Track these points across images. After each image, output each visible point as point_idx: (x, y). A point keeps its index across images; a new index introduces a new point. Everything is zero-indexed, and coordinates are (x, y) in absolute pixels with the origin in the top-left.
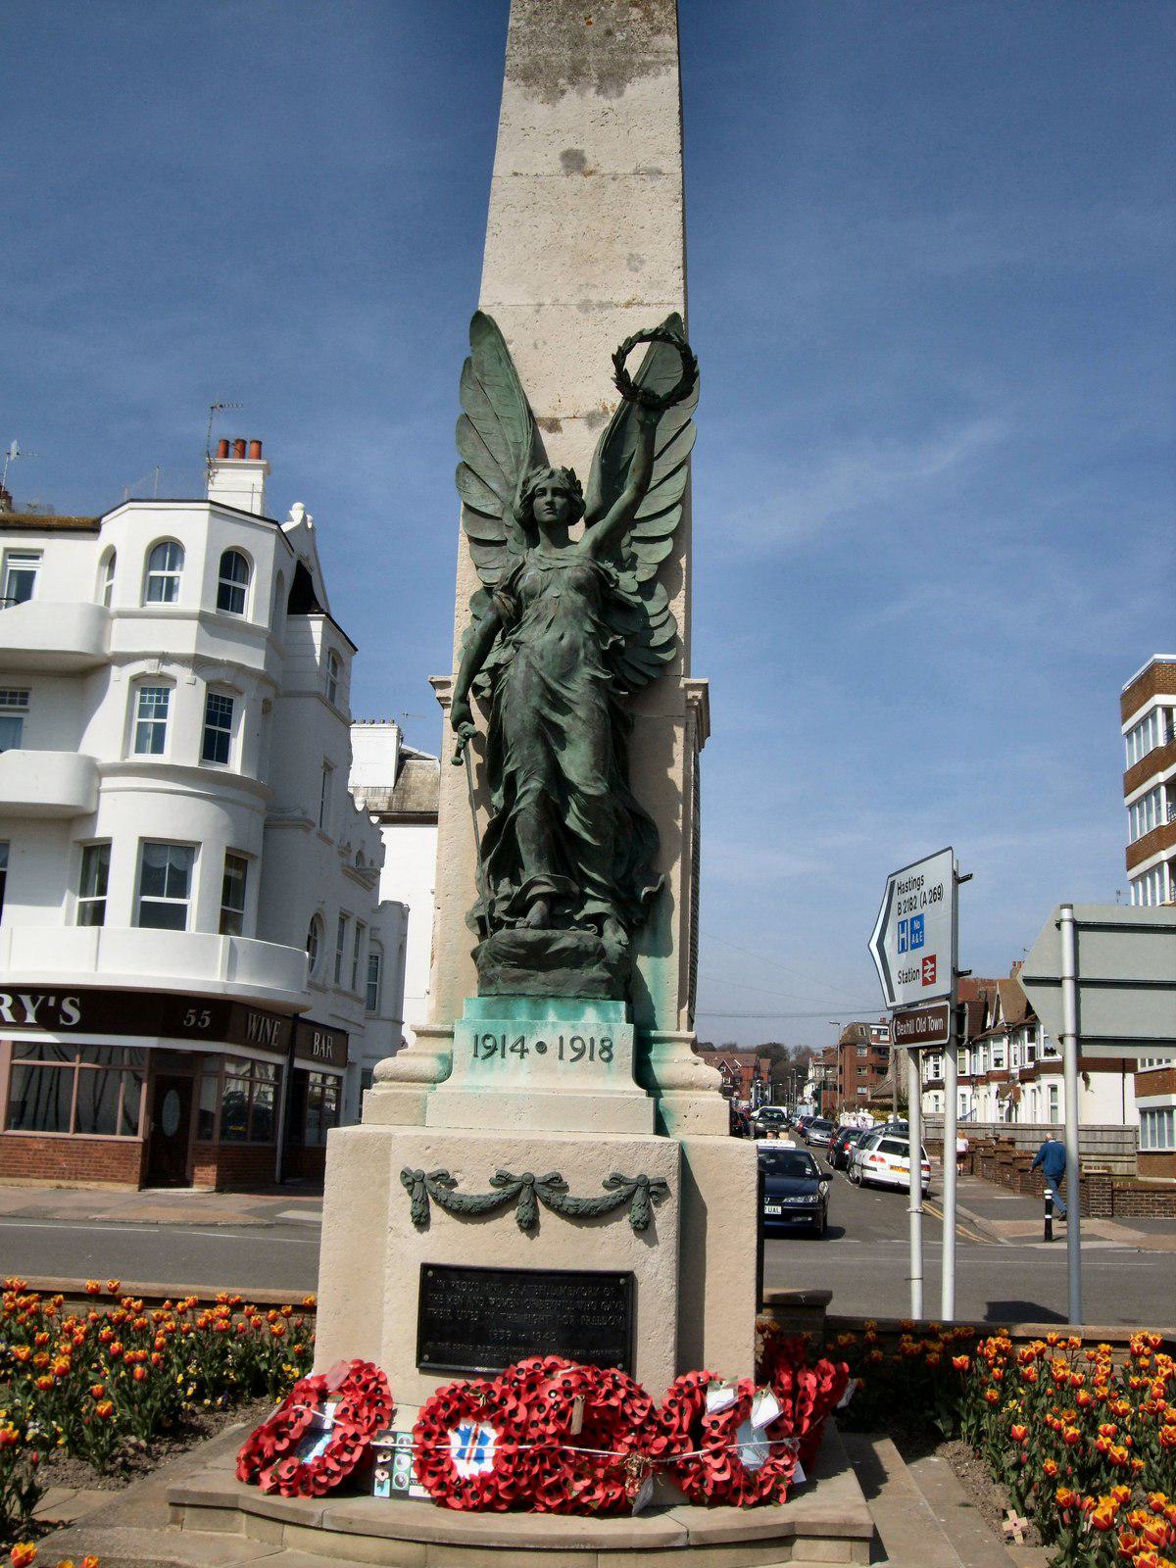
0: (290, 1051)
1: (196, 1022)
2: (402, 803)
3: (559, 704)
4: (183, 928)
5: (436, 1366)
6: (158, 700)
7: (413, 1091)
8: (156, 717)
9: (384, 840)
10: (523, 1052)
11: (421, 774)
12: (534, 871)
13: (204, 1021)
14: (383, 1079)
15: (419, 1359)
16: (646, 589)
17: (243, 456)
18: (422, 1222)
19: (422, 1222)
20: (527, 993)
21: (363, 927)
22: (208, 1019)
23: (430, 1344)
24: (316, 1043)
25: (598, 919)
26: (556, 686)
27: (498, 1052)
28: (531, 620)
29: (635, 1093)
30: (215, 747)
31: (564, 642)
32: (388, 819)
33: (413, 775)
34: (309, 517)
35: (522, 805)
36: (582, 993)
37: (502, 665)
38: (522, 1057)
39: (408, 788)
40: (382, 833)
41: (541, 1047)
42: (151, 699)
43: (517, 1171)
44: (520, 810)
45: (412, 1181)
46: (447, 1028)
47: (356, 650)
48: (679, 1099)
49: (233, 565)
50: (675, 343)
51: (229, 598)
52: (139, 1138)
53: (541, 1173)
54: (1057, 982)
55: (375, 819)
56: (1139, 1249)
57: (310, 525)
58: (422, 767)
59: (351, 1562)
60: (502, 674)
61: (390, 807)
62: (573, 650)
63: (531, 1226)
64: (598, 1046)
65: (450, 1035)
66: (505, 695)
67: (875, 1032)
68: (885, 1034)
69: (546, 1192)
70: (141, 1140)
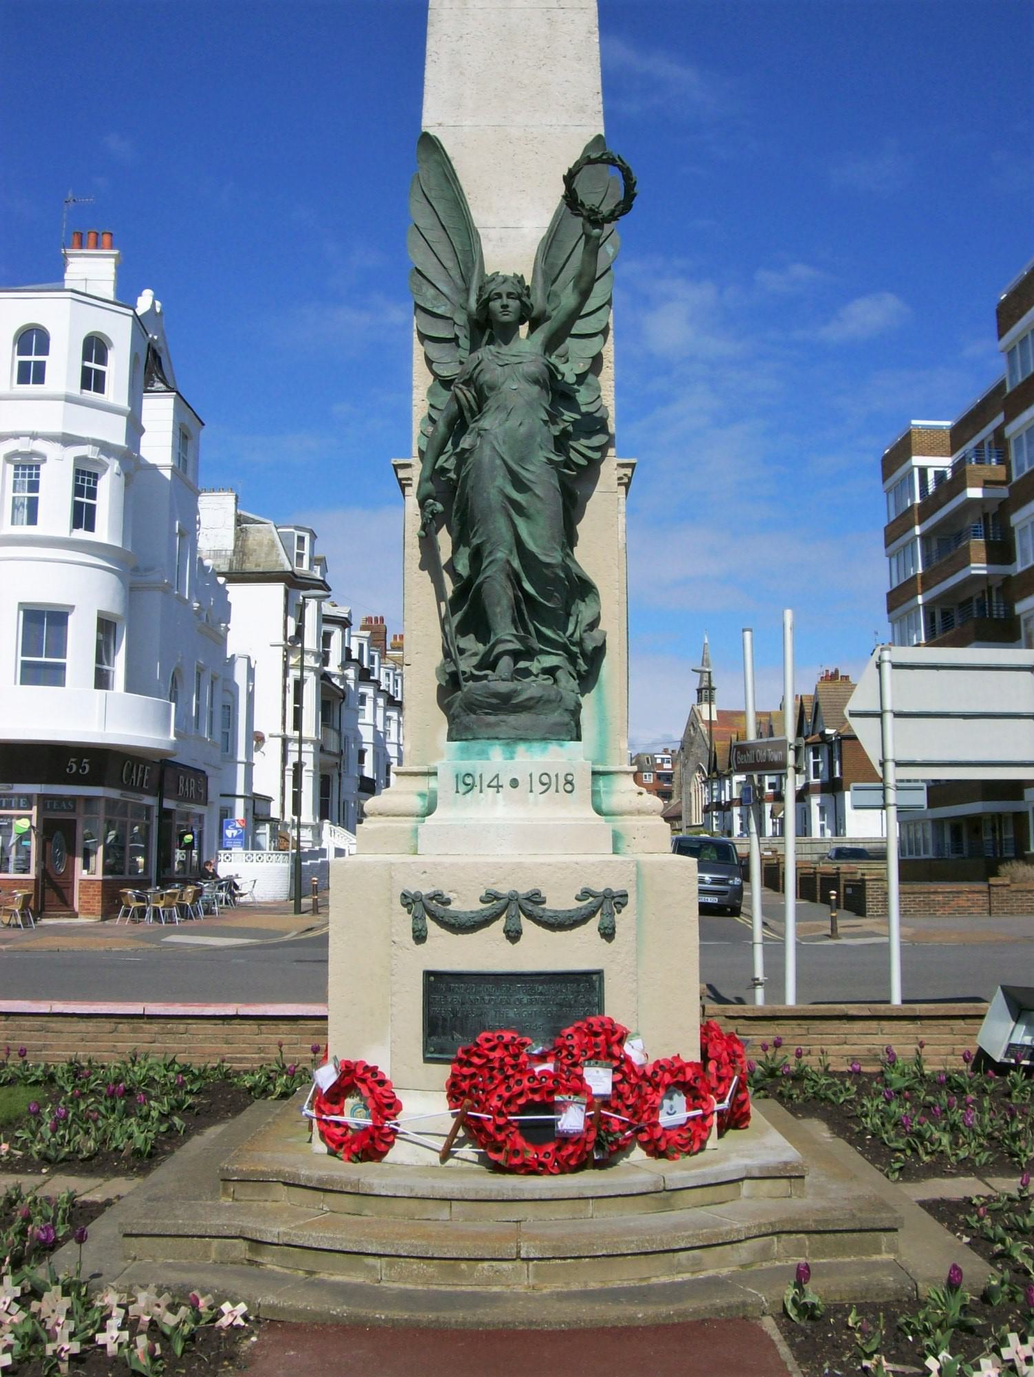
0: (161, 794)
1: (78, 770)
3: (520, 484)
4: (63, 685)
5: (441, 1056)
6: (30, 475)
7: (648, 823)
8: (29, 492)
9: (230, 598)
10: (499, 787)
11: (258, 537)
12: (505, 633)
13: (84, 768)
14: (372, 815)
15: (426, 1050)
16: (581, 378)
17: (97, 246)
18: (420, 937)
19: (420, 937)
21: (216, 678)
22: (87, 766)
23: (434, 1038)
24: (181, 785)
25: (551, 671)
26: (516, 467)
27: (477, 789)
28: (493, 409)
29: (594, 819)
30: (83, 516)
31: (522, 430)
32: (239, 576)
34: (158, 303)
35: (488, 573)
36: (548, 735)
37: (467, 450)
39: (246, 551)
40: (227, 592)
41: (514, 783)
42: (24, 476)
43: (504, 889)
44: (486, 578)
45: (409, 900)
47: (203, 424)
48: (619, 824)
49: (95, 347)
50: (618, 166)
51: (93, 380)
52: (32, 875)
53: (524, 890)
54: (897, 715)
55: (221, 580)
56: (911, 942)
57: (158, 310)
58: (259, 531)
60: (468, 458)
61: (230, 568)
62: (530, 436)
63: (513, 935)
64: (562, 781)
65: (594, 773)
66: (473, 475)
67: (659, 761)
68: (668, 762)
69: (530, 907)
70: (34, 877)
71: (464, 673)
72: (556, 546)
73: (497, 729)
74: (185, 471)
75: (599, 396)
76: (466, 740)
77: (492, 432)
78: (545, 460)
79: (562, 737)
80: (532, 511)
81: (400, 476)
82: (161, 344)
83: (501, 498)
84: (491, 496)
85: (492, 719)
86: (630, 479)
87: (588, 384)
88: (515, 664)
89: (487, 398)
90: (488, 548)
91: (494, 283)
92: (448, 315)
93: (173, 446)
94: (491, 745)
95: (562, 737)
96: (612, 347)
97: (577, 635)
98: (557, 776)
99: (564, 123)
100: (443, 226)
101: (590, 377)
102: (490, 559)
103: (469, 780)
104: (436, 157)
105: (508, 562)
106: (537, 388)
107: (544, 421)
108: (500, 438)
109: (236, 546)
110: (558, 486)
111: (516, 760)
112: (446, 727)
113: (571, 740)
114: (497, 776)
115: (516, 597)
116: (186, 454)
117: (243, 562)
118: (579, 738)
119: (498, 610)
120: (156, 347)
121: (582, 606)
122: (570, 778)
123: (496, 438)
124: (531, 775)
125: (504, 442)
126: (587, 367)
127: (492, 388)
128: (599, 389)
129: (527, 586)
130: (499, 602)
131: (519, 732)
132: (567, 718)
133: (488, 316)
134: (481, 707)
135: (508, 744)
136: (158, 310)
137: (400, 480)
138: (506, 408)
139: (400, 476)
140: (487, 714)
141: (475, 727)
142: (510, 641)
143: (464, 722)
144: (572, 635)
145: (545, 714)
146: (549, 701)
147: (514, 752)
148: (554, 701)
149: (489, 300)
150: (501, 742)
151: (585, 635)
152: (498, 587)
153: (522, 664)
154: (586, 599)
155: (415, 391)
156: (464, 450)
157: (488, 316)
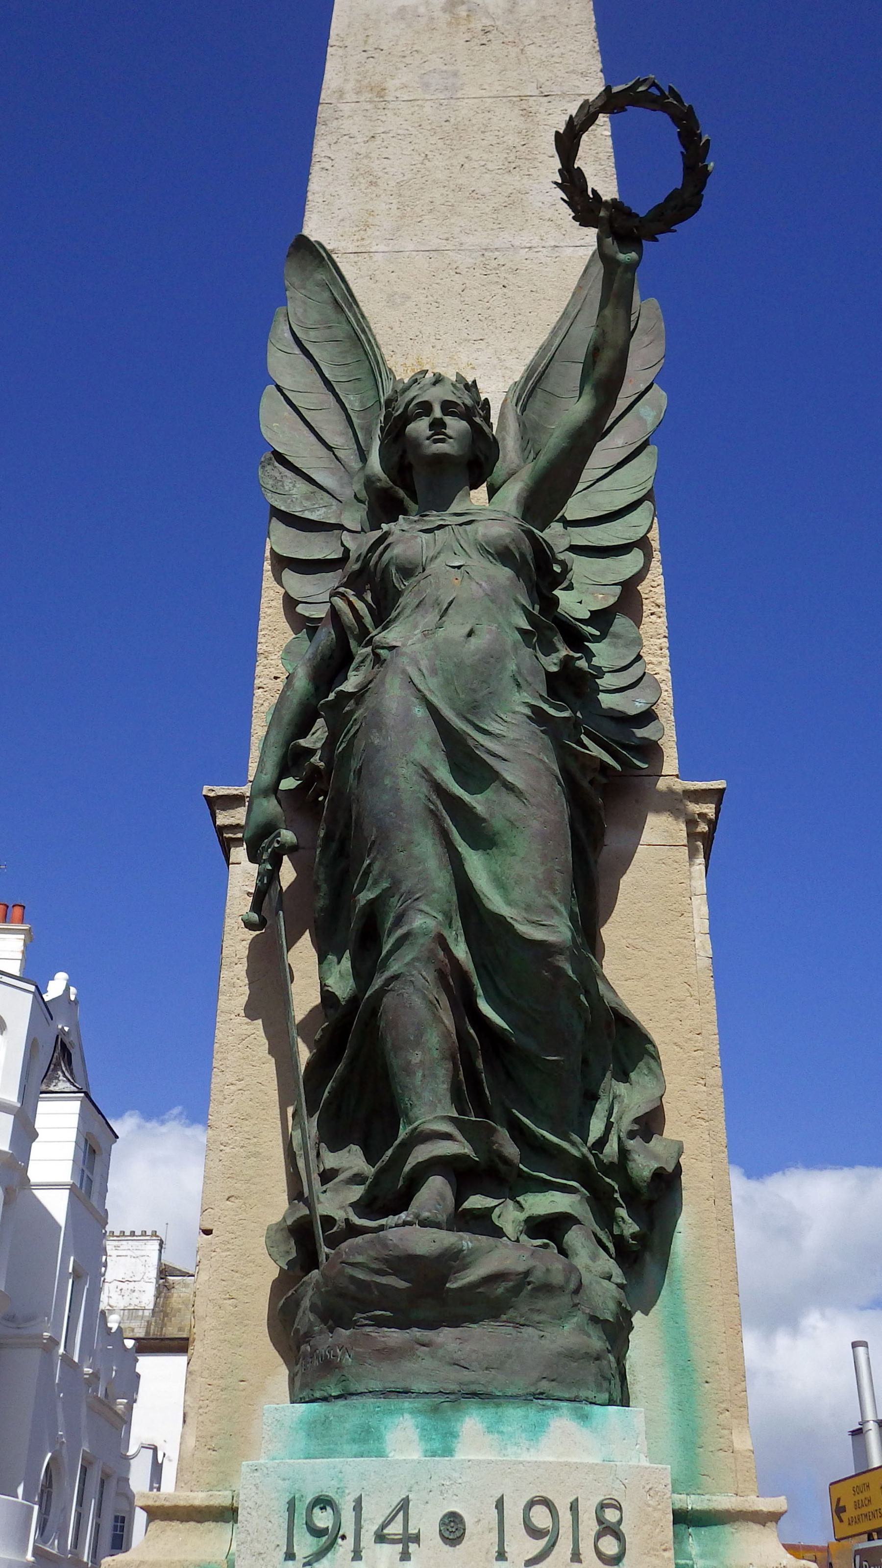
2: (162, 1329)
9: (138, 1369)
10: (409, 1539)
20: (415, 1387)
21: (91, 1463)
27: (345, 1547)
28: (408, 612)
33: (175, 1295)
34: (73, 990)
35: (395, 967)
36: (544, 1385)
37: (350, 695)
38: (405, 1556)
39: (168, 1310)
43: (762, 1527)
46: (221, 1498)
47: (117, 1137)
57: (73, 998)
58: (186, 1285)
59: (378, 676)
60: (352, 712)
61: (147, 1333)
64: (589, 1525)
71: (328, 1221)
72: (555, 901)
73: (408, 1365)
74: (89, 1192)
75: (639, 657)
76: (325, 1399)
77: (407, 650)
78: (528, 711)
79: (583, 1394)
80: (497, 823)
81: (219, 822)
82: (73, 1038)
83: (424, 789)
84: (402, 785)
85: (394, 1336)
86: (713, 825)
87: (617, 636)
88: (460, 1199)
89: (399, 594)
90: (395, 905)
91: (416, 387)
92: (333, 521)
93: (74, 1161)
94: (391, 1413)
95: (583, 1394)
96: (661, 580)
97: (611, 1148)
98: (574, 1507)
99: (553, 243)
100: (327, 383)
101: (621, 623)
102: (400, 932)
103: (323, 1519)
104: (320, 276)
105: (441, 940)
106: (504, 574)
107: (522, 632)
108: (424, 664)
109: (156, 1304)
110: (556, 768)
111: (459, 1456)
112: (283, 1373)
113: (611, 1403)
114: (404, 1506)
115: (461, 1034)
116: (92, 1173)
117: (164, 1325)
118: (625, 1402)
119: (416, 1057)
120: (66, 1041)
121: (621, 1088)
122: (611, 1515)
123: (416, 663)
124: (500, 1505)
125: (434, 672)
126: (612, 601)
127: (407, 571)
128: (638, 642)
129: (485, 1008)
130: (420, 1035)
131: (466, 1375)
132: (596, 1342)
133: (403, 456)
134: (364, 1306)
135: (435, 1409)
136: (73, 998)
137: (220, 830)
138: (436, 602)
139: (219, 822)
140: (380, 1323)
141: (348, 1360)
142: (448, 1137)
143: (322, 1350)
144: (601, 1142)
145: (535, 1325)
146: (547, 1289)
147: (454, 1435)
148: (562, 1289)
149: (406, 419)
150: (419, 1403)
151: (631, 1144)
152: (417, 1001)
153: (475, 1202)
154: (633, 1075)
155: (261, 660)
156: (344, 697)
157: (403, 456)
